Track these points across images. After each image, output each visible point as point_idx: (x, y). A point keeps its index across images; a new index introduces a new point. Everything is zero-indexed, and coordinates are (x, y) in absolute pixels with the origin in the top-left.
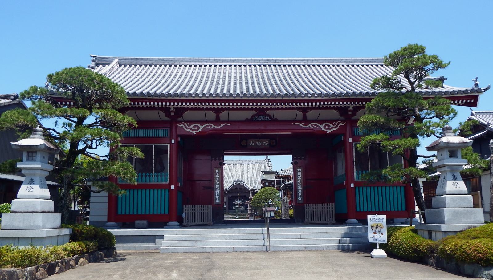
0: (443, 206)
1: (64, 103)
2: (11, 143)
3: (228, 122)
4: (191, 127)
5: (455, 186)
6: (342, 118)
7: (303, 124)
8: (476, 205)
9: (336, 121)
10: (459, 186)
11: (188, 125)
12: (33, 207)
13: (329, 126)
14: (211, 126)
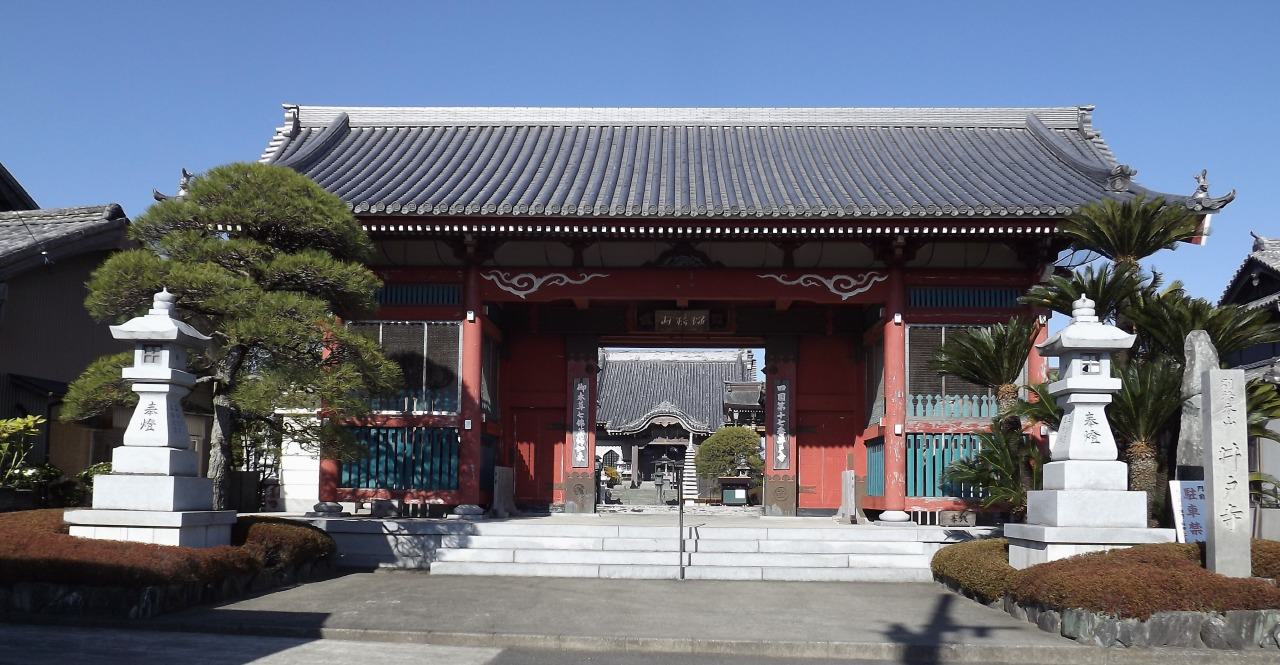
0: (1054, 485)
1: (220, 227)
3: (602, 269)
4: (515, 281)
5: (1091, 440)
6: (880, 264)
7: (784, 278)
9: (865, 270)
10: (1099, 438)
11: (506, 277)
14: (562, 280)
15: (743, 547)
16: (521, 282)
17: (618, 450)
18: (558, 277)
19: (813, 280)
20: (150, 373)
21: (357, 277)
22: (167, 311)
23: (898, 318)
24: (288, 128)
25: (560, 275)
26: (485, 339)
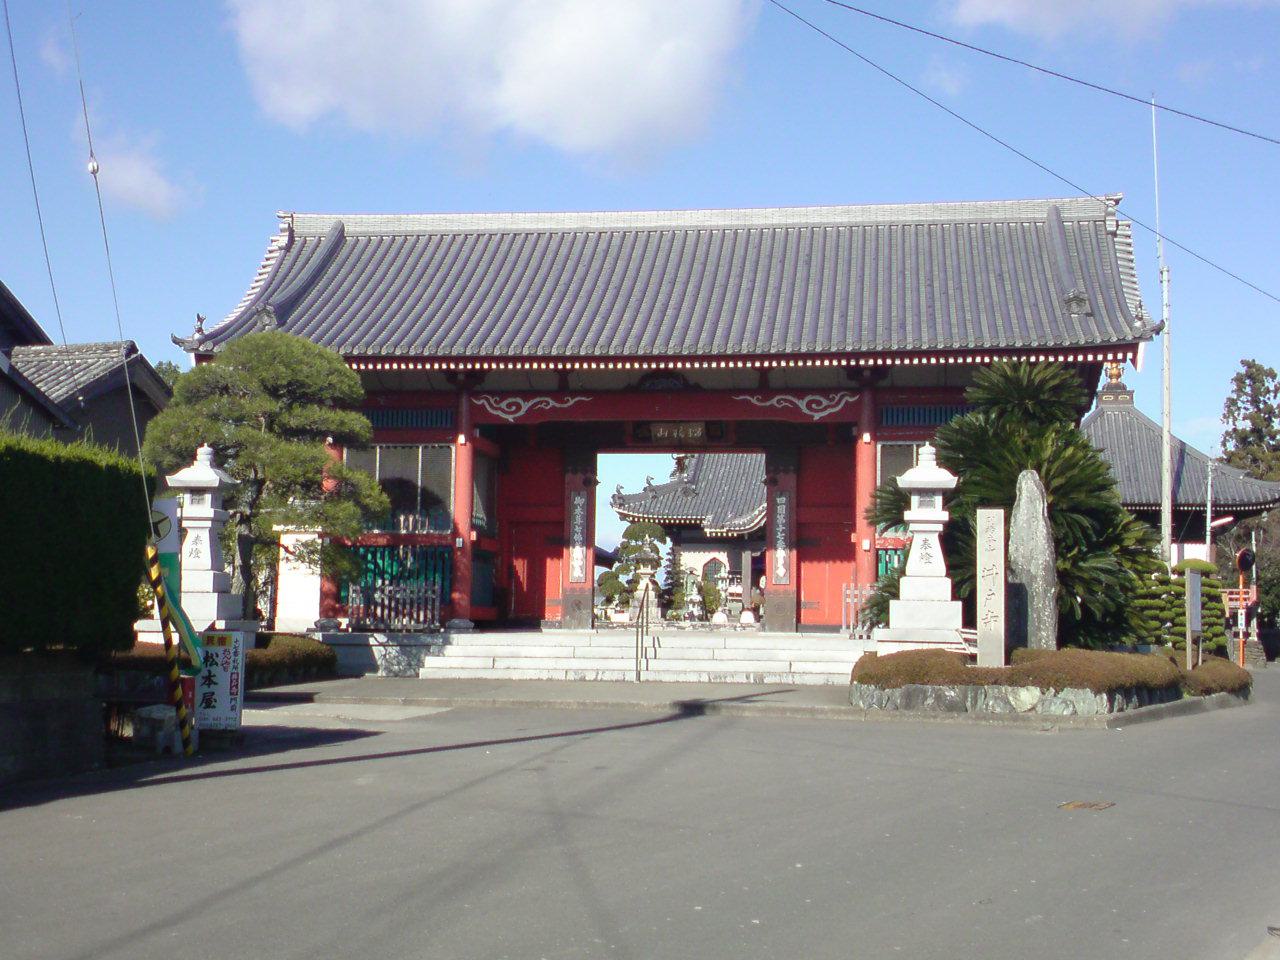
2: (525, 589)
4: (503, 405)
8: (955, 597)
9: (837, 390)
10: (931, 560)
11: (496, 401)
12: (1278, 437)
13: (819, 403)
15: (701, 654)
16: (509, 405)
17: (722, 557)
18: (546, 401)
19: (786, 401)
20: (198, 513)
21: (357, 422)
22: (208, 463)
23: (867, 437)
24: (284, 240)
25: (546, 399)
26: (477, 455)
